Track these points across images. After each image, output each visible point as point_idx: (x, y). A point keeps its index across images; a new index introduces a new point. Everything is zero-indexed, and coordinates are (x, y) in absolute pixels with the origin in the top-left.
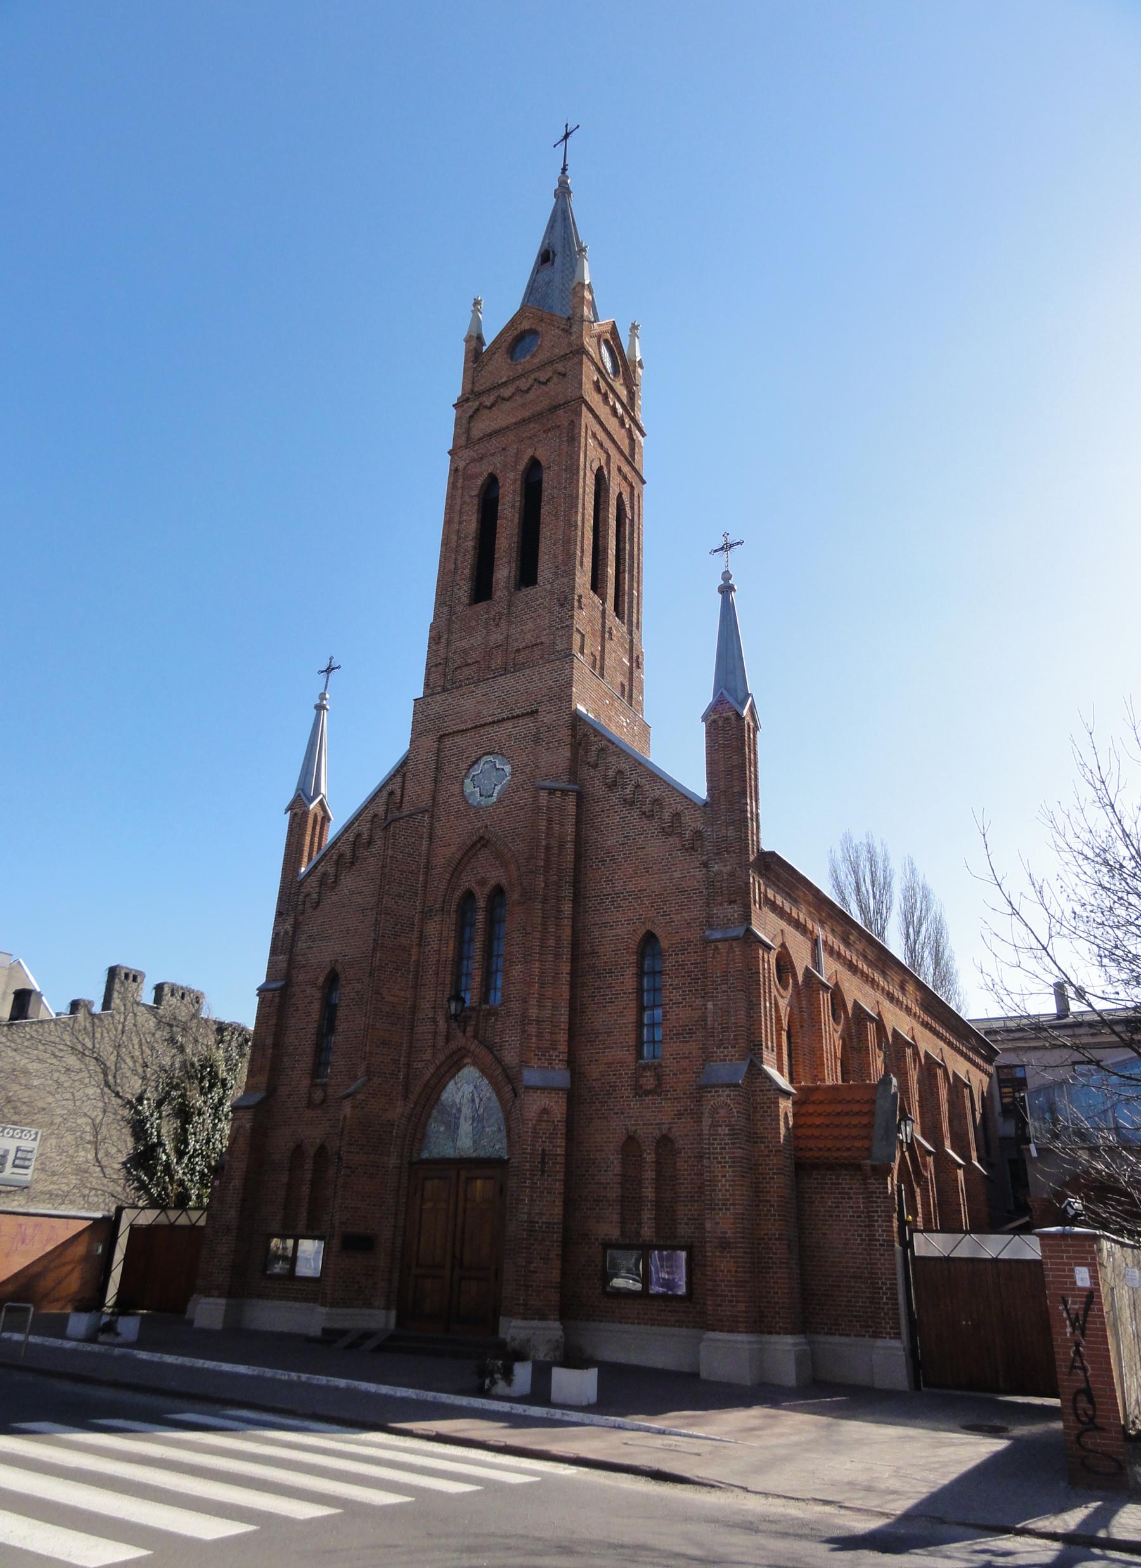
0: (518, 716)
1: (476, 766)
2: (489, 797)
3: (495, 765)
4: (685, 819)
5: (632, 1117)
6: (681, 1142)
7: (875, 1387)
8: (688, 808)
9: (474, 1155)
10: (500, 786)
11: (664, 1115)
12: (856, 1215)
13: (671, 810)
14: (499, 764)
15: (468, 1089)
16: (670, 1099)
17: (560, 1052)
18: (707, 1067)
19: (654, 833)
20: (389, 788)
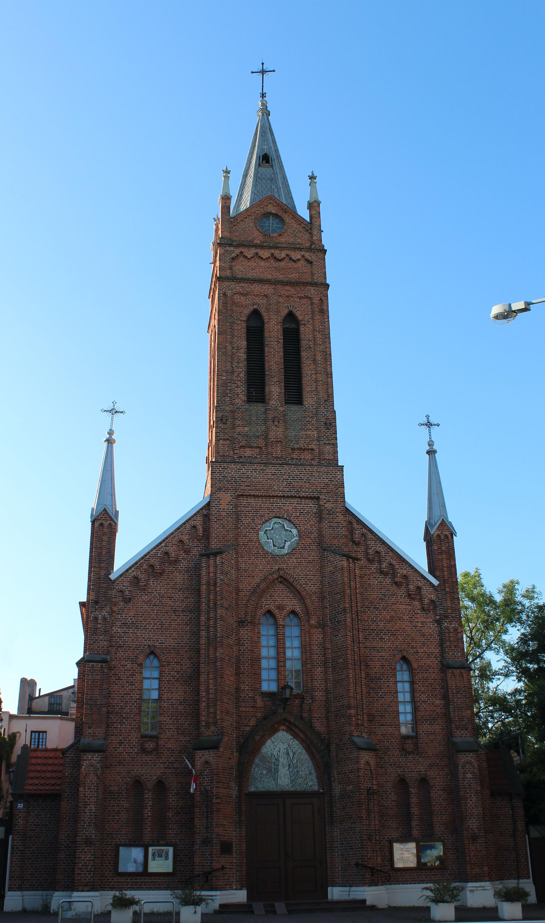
0: (303, 497)
1: (268, 524)
2: (281, 548)
3: (283, 526)
4: (424, 592)
5: (401, 767)
6: (433, 782)
7: (469, 906)
8: (425, 585)
9: (293, 789)
10: (289, 543)
11: (421, 766)
12: (505, 819)
13: (414, 584)
14: (287, 527)
15: (283, 747)
16: (424, 757)
17: (365, 727)
18: (106, 710)
19: (402, 596)
20: (192, 523)
